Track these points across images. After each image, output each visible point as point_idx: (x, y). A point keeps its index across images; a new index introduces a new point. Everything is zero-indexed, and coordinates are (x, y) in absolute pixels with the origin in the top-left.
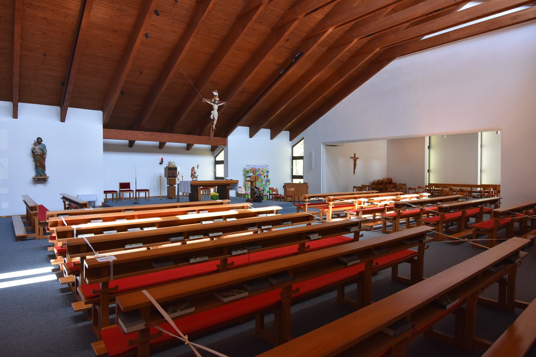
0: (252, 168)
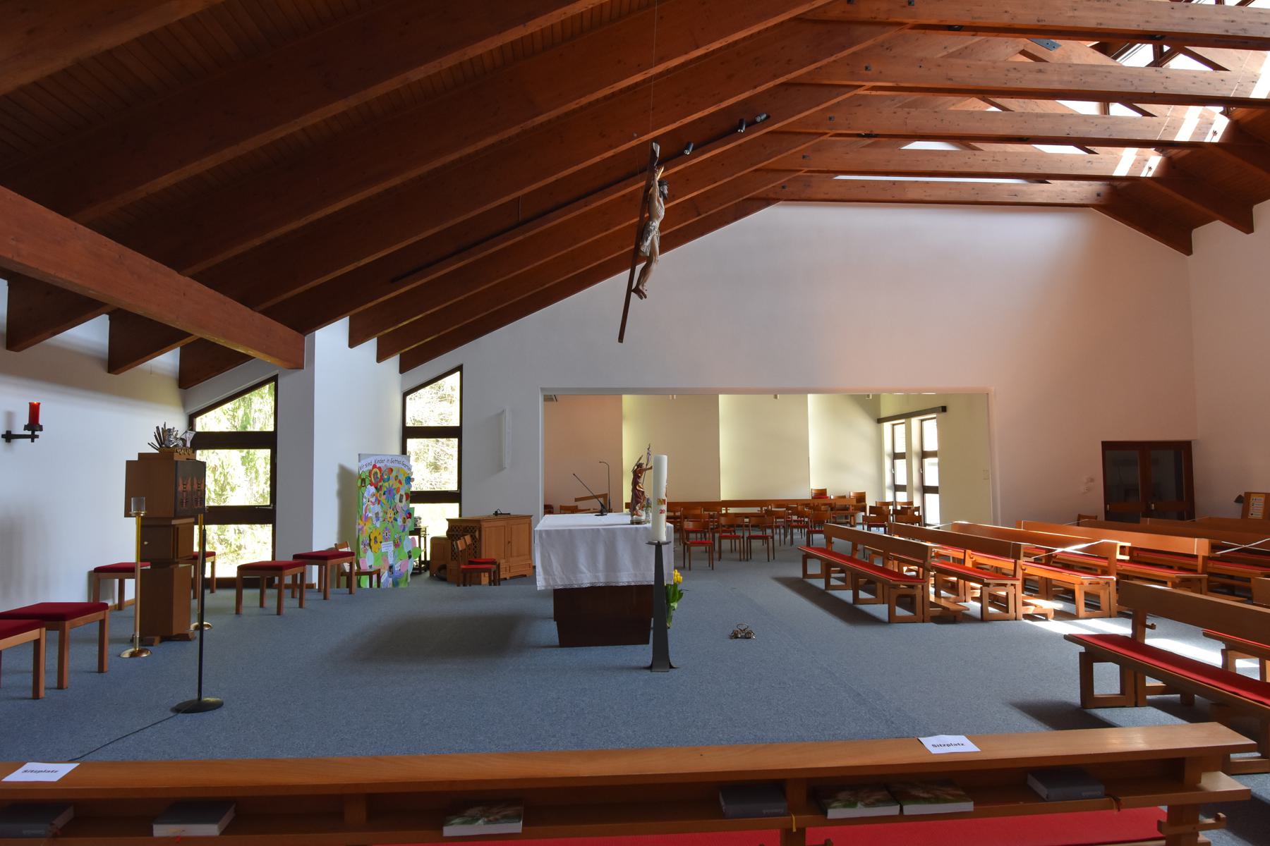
0: (375, 466)
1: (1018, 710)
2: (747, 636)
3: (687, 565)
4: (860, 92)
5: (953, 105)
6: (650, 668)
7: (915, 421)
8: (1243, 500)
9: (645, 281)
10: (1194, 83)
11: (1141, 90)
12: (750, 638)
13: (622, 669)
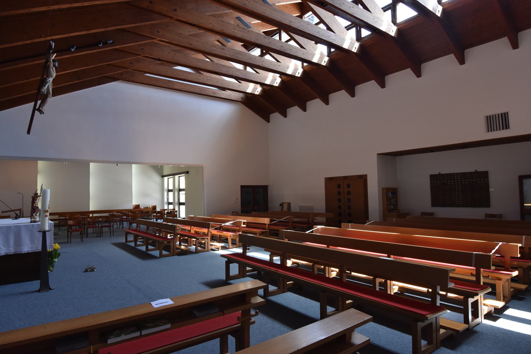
1: (204, 285)
2: (92, 270)
3: (69, 240)
4: (155, 41)
5: (193, 55)
6: (39, 291)
7: (177, 177)
8: (282, 205)
9: (44, 106)
10: (271, 65)
11: (255, 63)
12: (94, 271)
13: (23, 293)
